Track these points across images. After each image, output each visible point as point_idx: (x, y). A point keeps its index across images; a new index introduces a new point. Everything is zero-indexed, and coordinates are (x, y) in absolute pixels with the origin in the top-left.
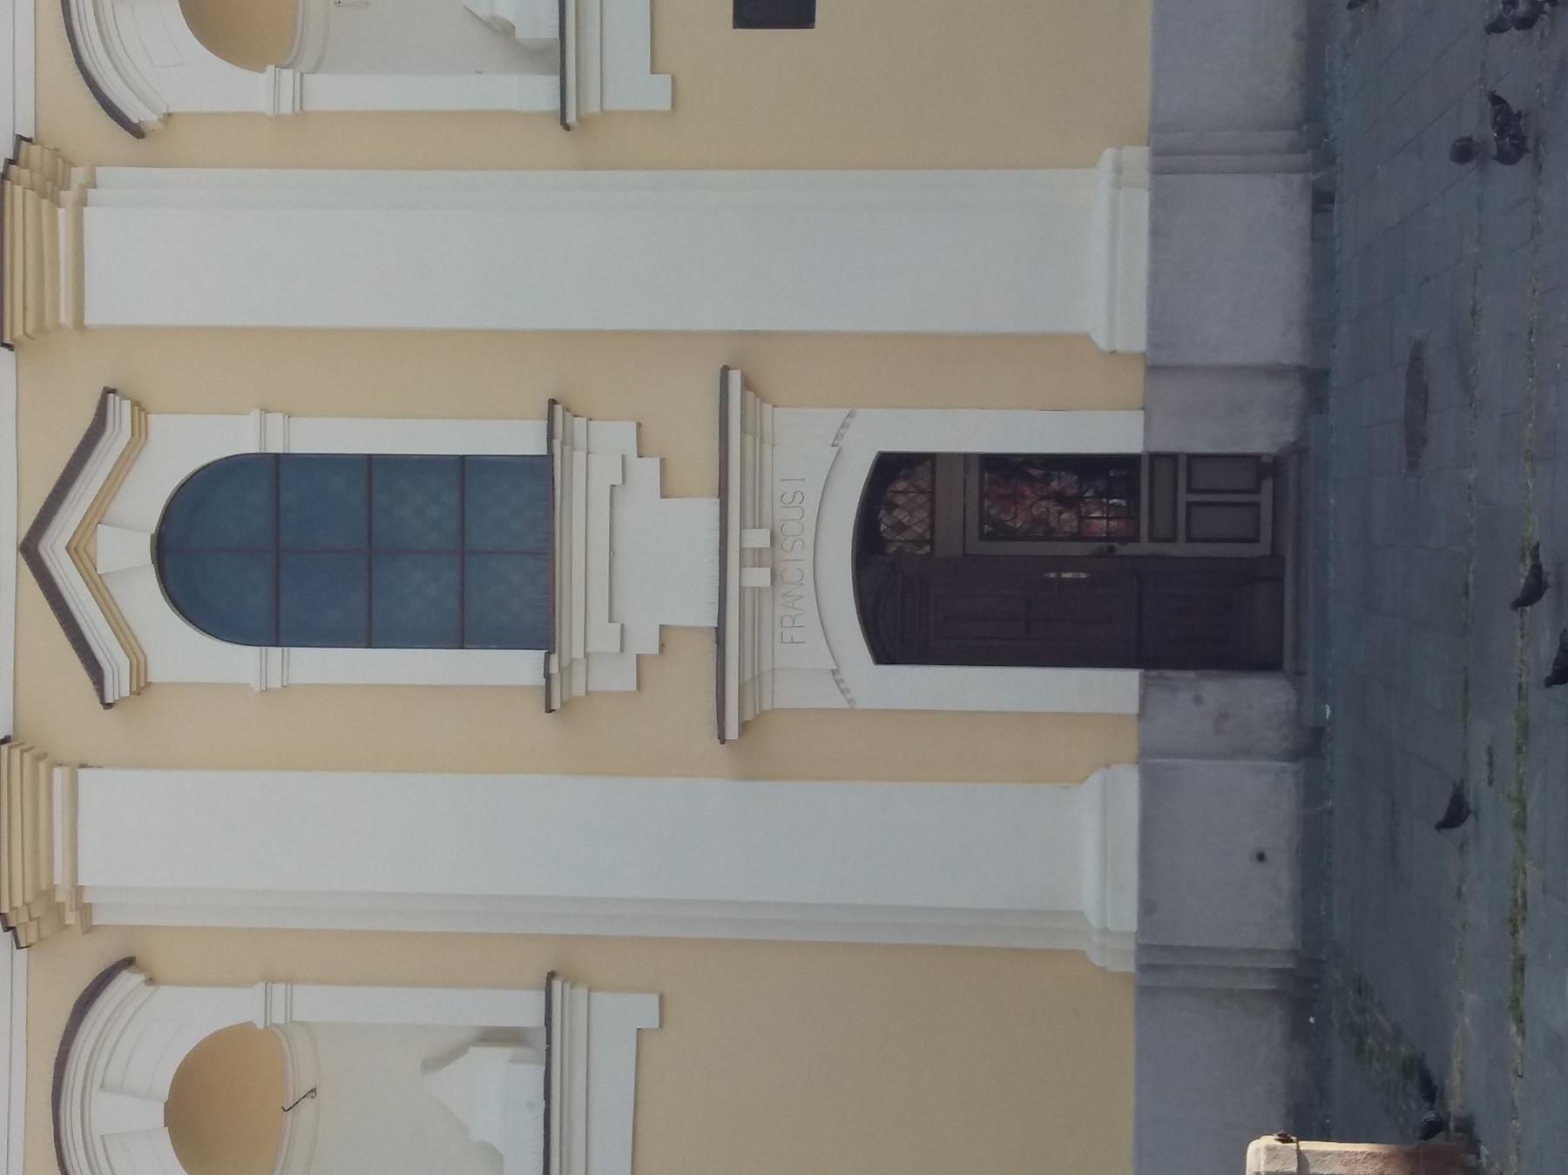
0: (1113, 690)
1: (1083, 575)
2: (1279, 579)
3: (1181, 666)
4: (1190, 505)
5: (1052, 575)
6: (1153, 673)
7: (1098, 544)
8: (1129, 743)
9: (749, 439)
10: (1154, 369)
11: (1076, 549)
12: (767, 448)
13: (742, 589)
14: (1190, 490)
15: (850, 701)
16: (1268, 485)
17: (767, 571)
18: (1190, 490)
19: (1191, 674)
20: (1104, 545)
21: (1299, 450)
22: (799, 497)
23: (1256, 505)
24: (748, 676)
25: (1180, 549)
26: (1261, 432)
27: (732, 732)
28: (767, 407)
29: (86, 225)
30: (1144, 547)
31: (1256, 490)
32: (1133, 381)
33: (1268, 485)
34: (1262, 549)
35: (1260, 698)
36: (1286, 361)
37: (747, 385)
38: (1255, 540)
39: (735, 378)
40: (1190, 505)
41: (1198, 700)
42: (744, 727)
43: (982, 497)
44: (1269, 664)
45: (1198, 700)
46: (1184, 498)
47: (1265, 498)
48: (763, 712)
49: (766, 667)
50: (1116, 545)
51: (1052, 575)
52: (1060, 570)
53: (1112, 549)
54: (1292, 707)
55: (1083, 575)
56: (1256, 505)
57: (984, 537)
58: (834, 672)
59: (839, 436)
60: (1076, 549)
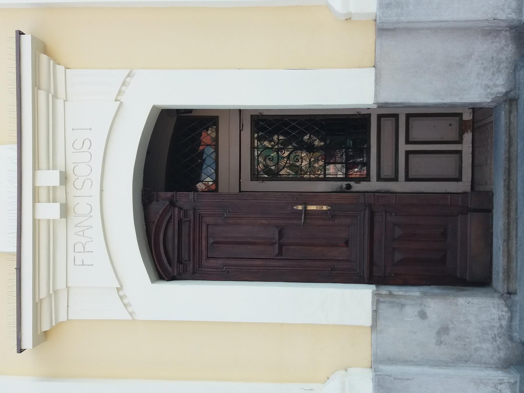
0: (350, 303)
1: (325, 208)
2: (487, 211)
3: (405, 283)
4: (408, 153)
5: (300, 208)
6: (385, 290)
7: (339, 183)
8: (364, 350)
9: (42, 94)
10: (384, 30)
11: (322, 187)
12: (60, 103)
13: (35, 223)
14: (408, 142)
15: (131, 314)
16: (468, 137)
17: (57, 206)
18: (408, 142)
19: (415, 292)
20: (344, 184)
21: (510, 100)
22: (87, 143)
23: (459, 152)
24: (43, 294)
25: (401, 186)
26: (474, 84)
27: (27, 342)
28: (60, 69)
29: (429, 191)
30: (373, 185)
31: (460, 142)
32: (367, 38)
33: (468, 137)
34: (464, 186)
35: (476, 313)
36: (502, 16)
37: (42, 48)
38: (459, 179)
39: (26, 40)
40: (408, 153)
41: (423, 315)
42: (42, 337)
43: (253, 148)
44: (478, 279)
45: (423, 315)
46: (403, 147)
47: (466, 147)
48: (59, 324)
49: (61, 285)
50: (352, 183)
51: (300, 208)
52: (305, 204)
53: (349, 187)
54: (504, 323)
55: (325, 208)
56: (459, 153)
57: (255, 176)
58: (118, 289)
59: (120, 93)
60: (322, 187)
